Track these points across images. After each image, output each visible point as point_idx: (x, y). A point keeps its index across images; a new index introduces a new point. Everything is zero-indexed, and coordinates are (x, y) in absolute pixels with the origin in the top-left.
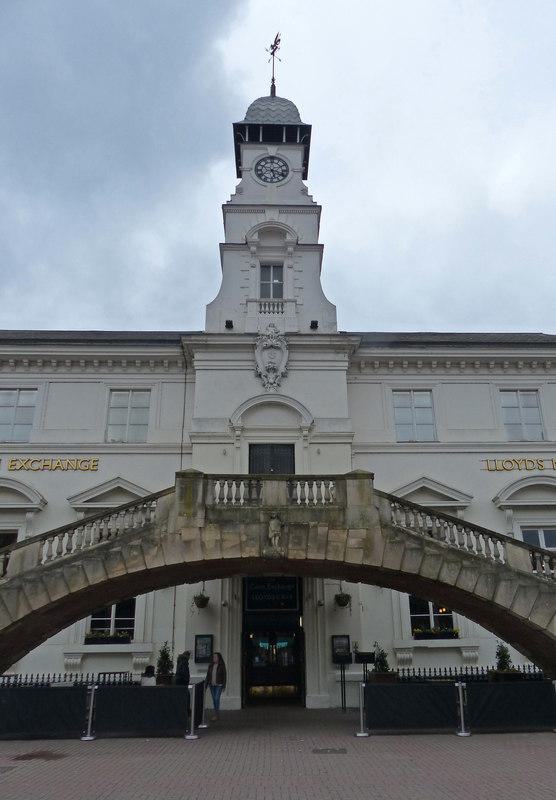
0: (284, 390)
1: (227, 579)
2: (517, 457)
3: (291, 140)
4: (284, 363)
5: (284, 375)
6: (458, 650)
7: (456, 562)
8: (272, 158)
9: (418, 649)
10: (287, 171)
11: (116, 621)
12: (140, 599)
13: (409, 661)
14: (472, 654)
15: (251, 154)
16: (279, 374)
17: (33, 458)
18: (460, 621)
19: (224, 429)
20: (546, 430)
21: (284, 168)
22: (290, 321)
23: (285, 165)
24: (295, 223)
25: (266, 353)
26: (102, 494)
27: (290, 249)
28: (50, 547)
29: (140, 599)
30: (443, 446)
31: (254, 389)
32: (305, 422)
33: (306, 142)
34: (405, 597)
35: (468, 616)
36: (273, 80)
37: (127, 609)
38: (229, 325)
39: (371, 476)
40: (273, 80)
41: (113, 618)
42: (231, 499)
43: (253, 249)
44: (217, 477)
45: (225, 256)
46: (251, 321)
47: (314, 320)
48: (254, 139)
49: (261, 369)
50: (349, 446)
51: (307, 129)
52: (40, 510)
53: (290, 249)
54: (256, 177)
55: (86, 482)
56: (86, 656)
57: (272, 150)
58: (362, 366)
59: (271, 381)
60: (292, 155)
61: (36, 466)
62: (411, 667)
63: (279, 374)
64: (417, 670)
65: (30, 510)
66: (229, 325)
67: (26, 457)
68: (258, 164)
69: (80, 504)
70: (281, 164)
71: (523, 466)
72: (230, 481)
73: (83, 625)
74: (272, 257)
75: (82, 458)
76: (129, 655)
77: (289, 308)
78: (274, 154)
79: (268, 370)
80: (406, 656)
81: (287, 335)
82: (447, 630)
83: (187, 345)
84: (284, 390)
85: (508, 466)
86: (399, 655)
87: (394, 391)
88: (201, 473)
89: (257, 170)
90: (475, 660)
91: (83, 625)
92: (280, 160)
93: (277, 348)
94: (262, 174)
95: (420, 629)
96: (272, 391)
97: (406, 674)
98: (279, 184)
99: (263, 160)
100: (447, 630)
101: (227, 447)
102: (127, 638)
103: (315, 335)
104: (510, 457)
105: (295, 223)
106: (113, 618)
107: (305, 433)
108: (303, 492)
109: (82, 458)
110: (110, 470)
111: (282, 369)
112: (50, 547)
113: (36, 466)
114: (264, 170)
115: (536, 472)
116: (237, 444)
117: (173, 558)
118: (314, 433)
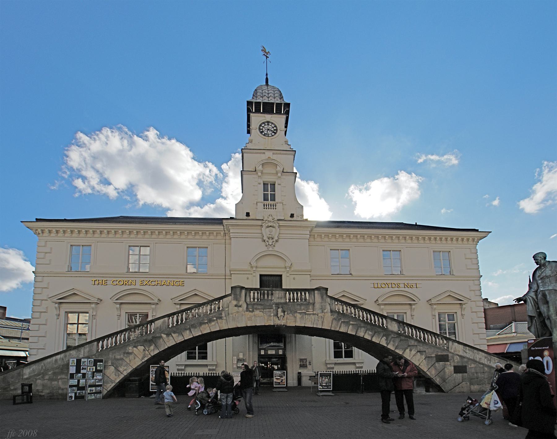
0: (276, 249)
1: (251, 335)
2: (388, 282)
3: (279, 112)
4: (277, 235)
5: (277, 241)
6: (354, 364)
7: (364, 327)
8: (268, 122)
9: (336, 364)
10: (276, 130)
11: (196, 350)
12: (209, 344)
13: (333, 368)
14: (361, 365)
15: (257, 119)
16: (274, 240)
17: (152, 280)
18: (355, 350)
19: (247, 267)
20: (403, 270)
21: (275, 128)
22: (280, 212)
23: (276, 126)
24: (283, 160)
25: (268, 229)
26: (68, 295)
27: (279, 175)
28: (173, 320)
29: (209, 344)
30: (209, 275)
31: (262, 248)
32: (288, 264)
33: (287, 113)
34: (332, 341)
35: (363, 350)
36: (267, 75)
37: (204, 348)
38: (248, 214)
39: (327, 289)
40: (267, 75)
41: (197, 351)
42: (291, 300)
43: (260, 174)
44: (252, 289)
45: (244, 176)
46: (259, 212)
47: (293, 213)
48: (258, 111)
49: (265, 238)
50: (309, 275)
51: (288, 105)
52: (158, 304)
53: (279, 175)
54: (260, 134)
55: (178, 292)
56: (186, 366)
57: (268, 117)
58: (316, 237)
59: (271, 244)
60: (278, 120)
61: (153, 283)
62: (362, 370)
63: (274, 240)
64: (188, 373)
65: (153, 304)
66: (248, 214)
67: (148, 279)
68: (260, 125)
69: (177, 301)
70: (273, 126)
71: (390, 286)
72: (254, 291)
73: (184, 354)
74: (269, 179)
75: (176, 280)
76: (206, 366)
77: (279, 206)
78: (269, 120)
79: (269, 238)
80: (332, 366)
81: (279, 220)
82: (349, 354)
83: (227, 225)
84: (276, 249)
85: (383, 286)
86: (328, 366)
87: (331, 250)
88: (244, 287)
89: (260, 129)
90: (362, 367)
91: (184, 354)
92: (272, 123)
93: (273, 227)
94: (263, 132)
95: (337, 355)
96: (271, 249)
97: (210, 375)
98: (272, 137)
99: (264, 123)
100: (349, 354)
101: (249, 276)
102: (205, 358)
103: (249, 219)
104: (385, 282)
105: (283, 160)
106: (197, 351)
107: (288, 269)
108: (293, 296)
109: (176, 280)
110: (190, 286)
111: (276, 238)
112: (173, 320)
113: (153, 283)
114: (264, 129)
115: (397, 289)
116: (254, 274)
117: (232, 325)
118: (292, 269)
